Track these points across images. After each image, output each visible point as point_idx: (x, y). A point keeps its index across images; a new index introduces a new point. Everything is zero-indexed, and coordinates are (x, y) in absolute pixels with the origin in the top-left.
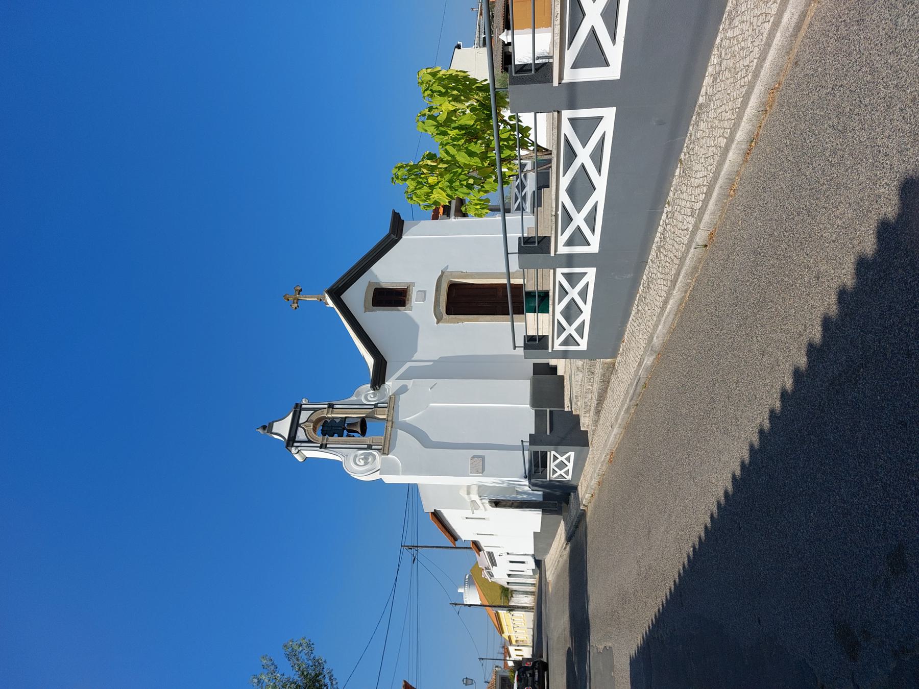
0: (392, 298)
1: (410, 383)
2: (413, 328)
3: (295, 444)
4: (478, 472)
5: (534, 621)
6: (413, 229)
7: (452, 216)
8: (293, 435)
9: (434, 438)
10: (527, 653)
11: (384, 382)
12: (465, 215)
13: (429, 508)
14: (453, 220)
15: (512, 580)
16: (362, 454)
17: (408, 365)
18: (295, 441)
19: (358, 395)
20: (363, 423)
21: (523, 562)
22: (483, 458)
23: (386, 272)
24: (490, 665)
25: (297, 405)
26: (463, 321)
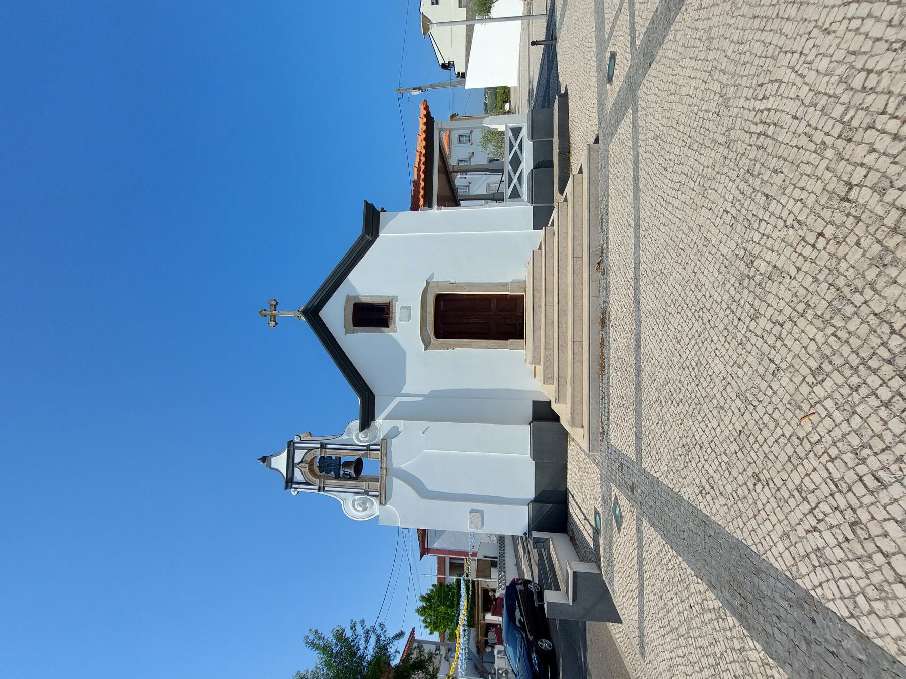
0: (372, 315)
1: (401, 424)
2: (400, 355)
3: (294, 486)
6: (391, 224)
7: (435, 206)
9: (430, 487)
11: (373, 419)
12: (452, 199)
14: (437, 212)
16: (359, 500)
17: (398, 400)
18: (293, 483)
19: (349, 433)
20: (358, 465)
23: (366, 282)
26: (453, 346)
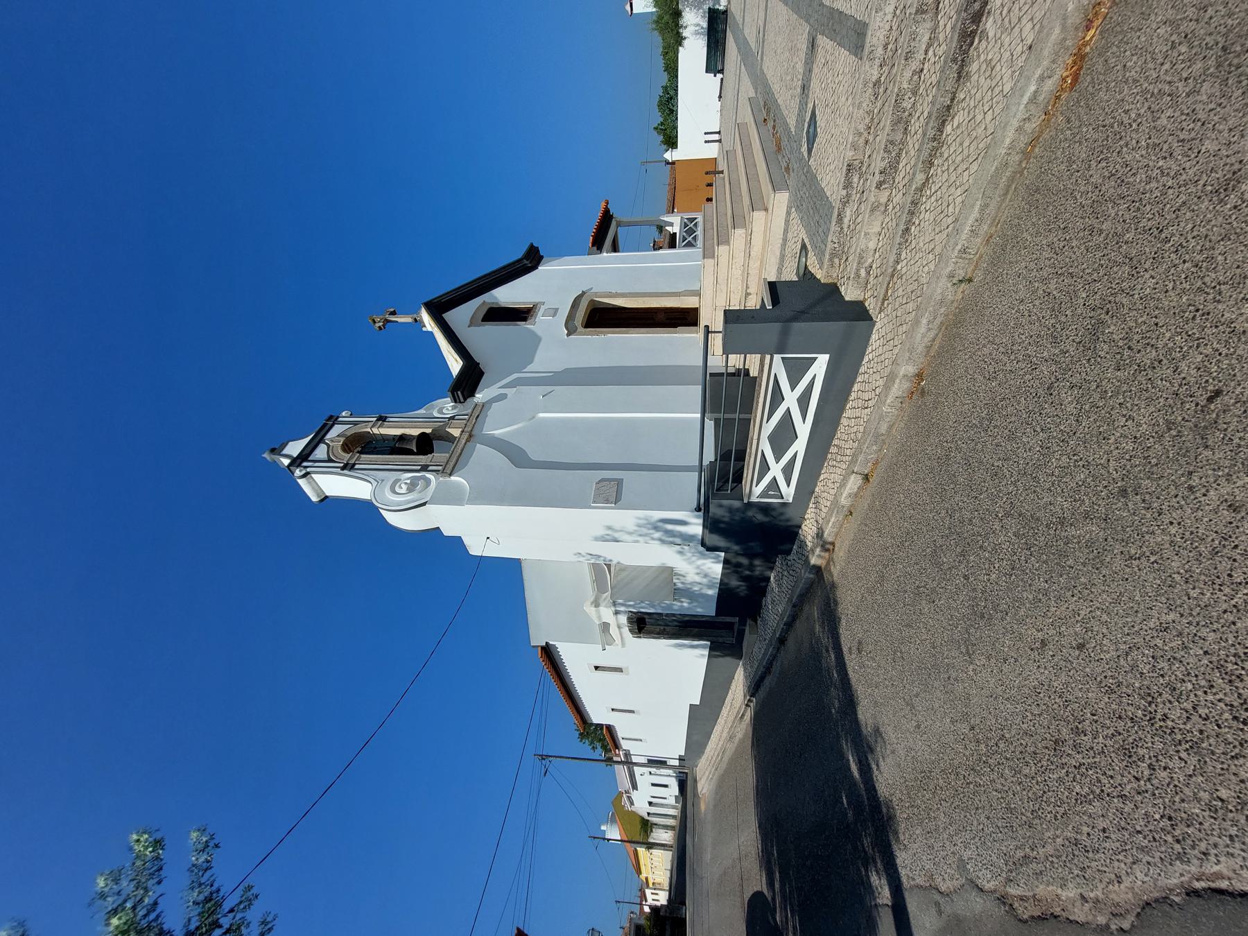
2: (536, 340)
4: (607, 501)
5: (672, 862)
8: (306, 452)
9: (535, 455)
10: (662, 898)
13: (538, 640)
15: (653, 810)
21: (666, 786)
22: (619, 483)
24: (626, 909)
25: (331, 417)
